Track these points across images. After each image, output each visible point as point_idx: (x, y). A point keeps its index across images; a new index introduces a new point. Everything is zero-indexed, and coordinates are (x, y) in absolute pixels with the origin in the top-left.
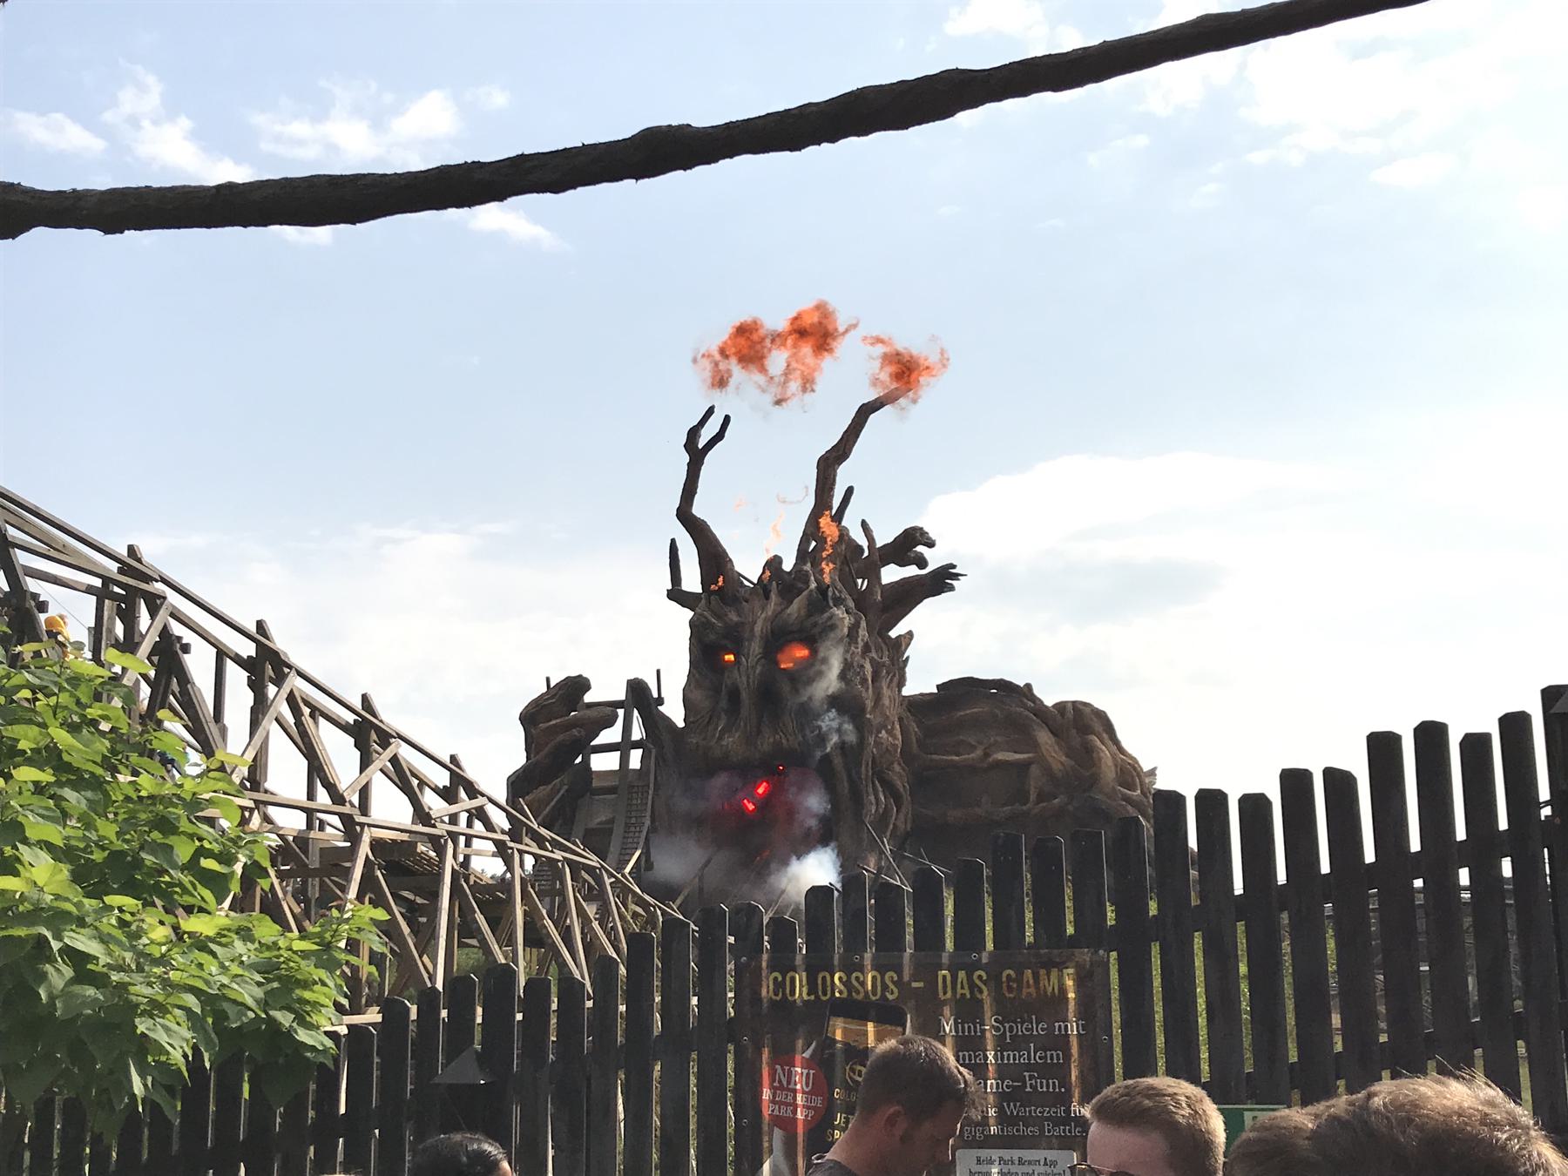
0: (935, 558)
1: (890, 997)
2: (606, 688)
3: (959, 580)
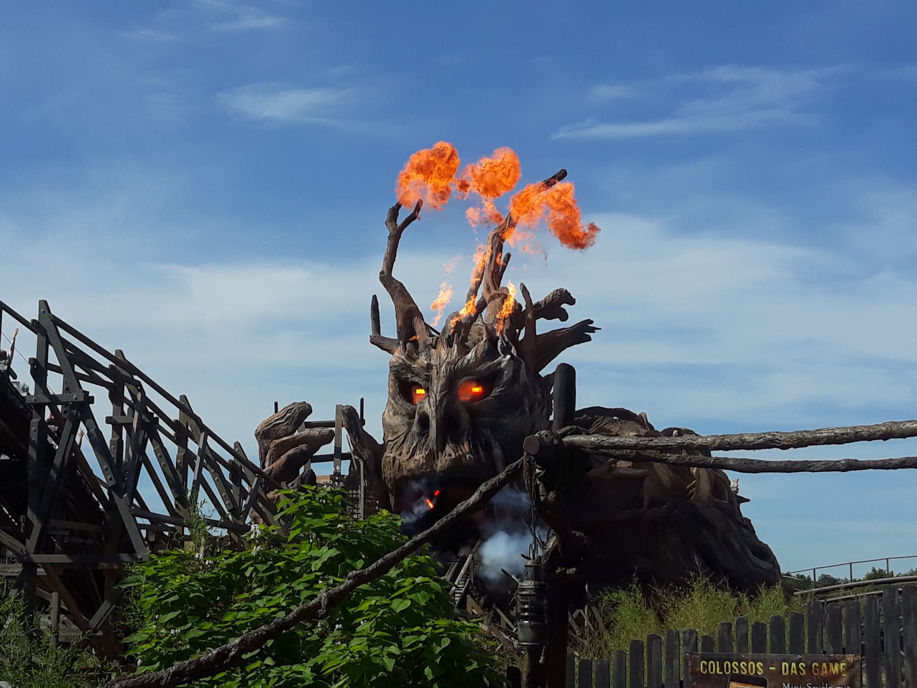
0: (575, 315)
1: (759, 673)
2: (323, 412)
3: (594, 332)
